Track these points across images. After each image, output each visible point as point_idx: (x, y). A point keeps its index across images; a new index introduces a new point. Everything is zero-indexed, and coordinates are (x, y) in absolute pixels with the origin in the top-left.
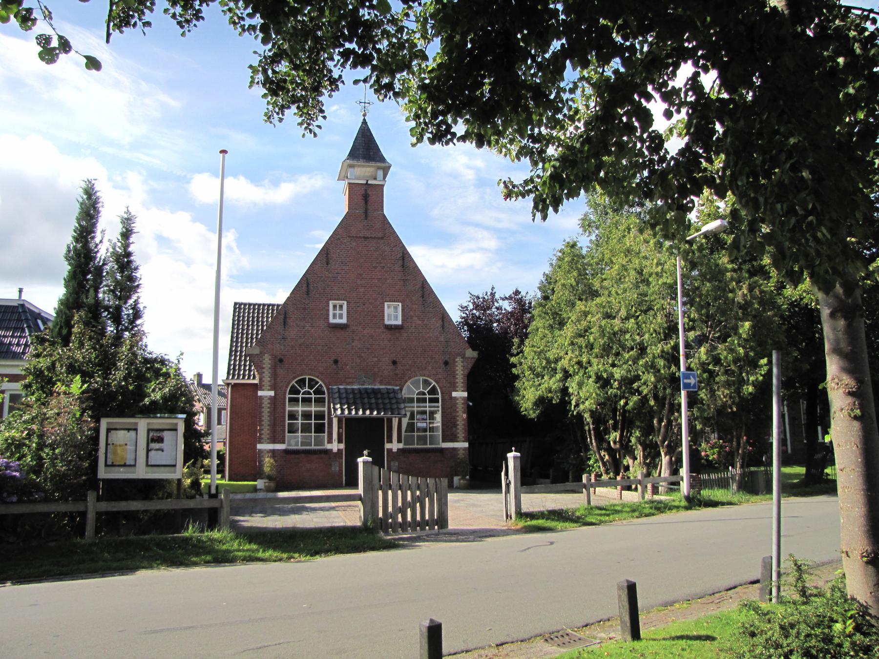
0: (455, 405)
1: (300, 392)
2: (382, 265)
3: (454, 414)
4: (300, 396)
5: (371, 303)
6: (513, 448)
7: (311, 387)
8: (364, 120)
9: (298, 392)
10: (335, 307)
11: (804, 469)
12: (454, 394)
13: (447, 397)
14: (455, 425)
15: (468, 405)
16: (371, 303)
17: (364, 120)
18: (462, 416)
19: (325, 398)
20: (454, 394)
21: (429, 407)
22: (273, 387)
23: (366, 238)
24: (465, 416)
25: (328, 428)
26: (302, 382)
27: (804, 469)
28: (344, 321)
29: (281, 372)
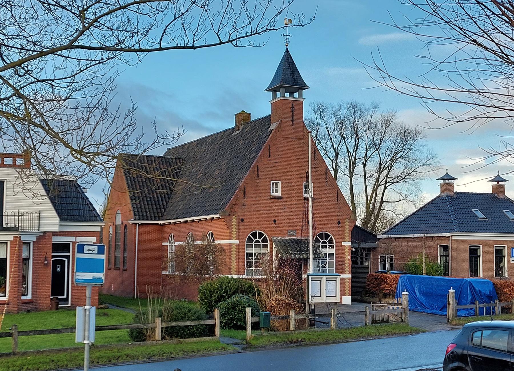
0: (344, 250)
1: (253, 240)
2: (302, 157)
3: (343, 256)
4: (254, 243)
5: (295, 183)
6: (452, 288)
7: (260, 238)
8: (287, 49)
9: (252, 241)
10: (273, 184)
11: (95, 238)
12: (343, 243)
13: (339, 245)
14: (343, 263)
15: (352, 250)
16: (295, 183)
17: (287, 49)
18: (348, 258)
19: (267, 245)
20: (343, 243)
21: (252, 259)
22: (238, 238)
23: (293, 139)
24: (349, 257)
25: (73, 248)
26: (254, 235)
27: (95, 238)
28: (279, 194)
29: (242, 228)
